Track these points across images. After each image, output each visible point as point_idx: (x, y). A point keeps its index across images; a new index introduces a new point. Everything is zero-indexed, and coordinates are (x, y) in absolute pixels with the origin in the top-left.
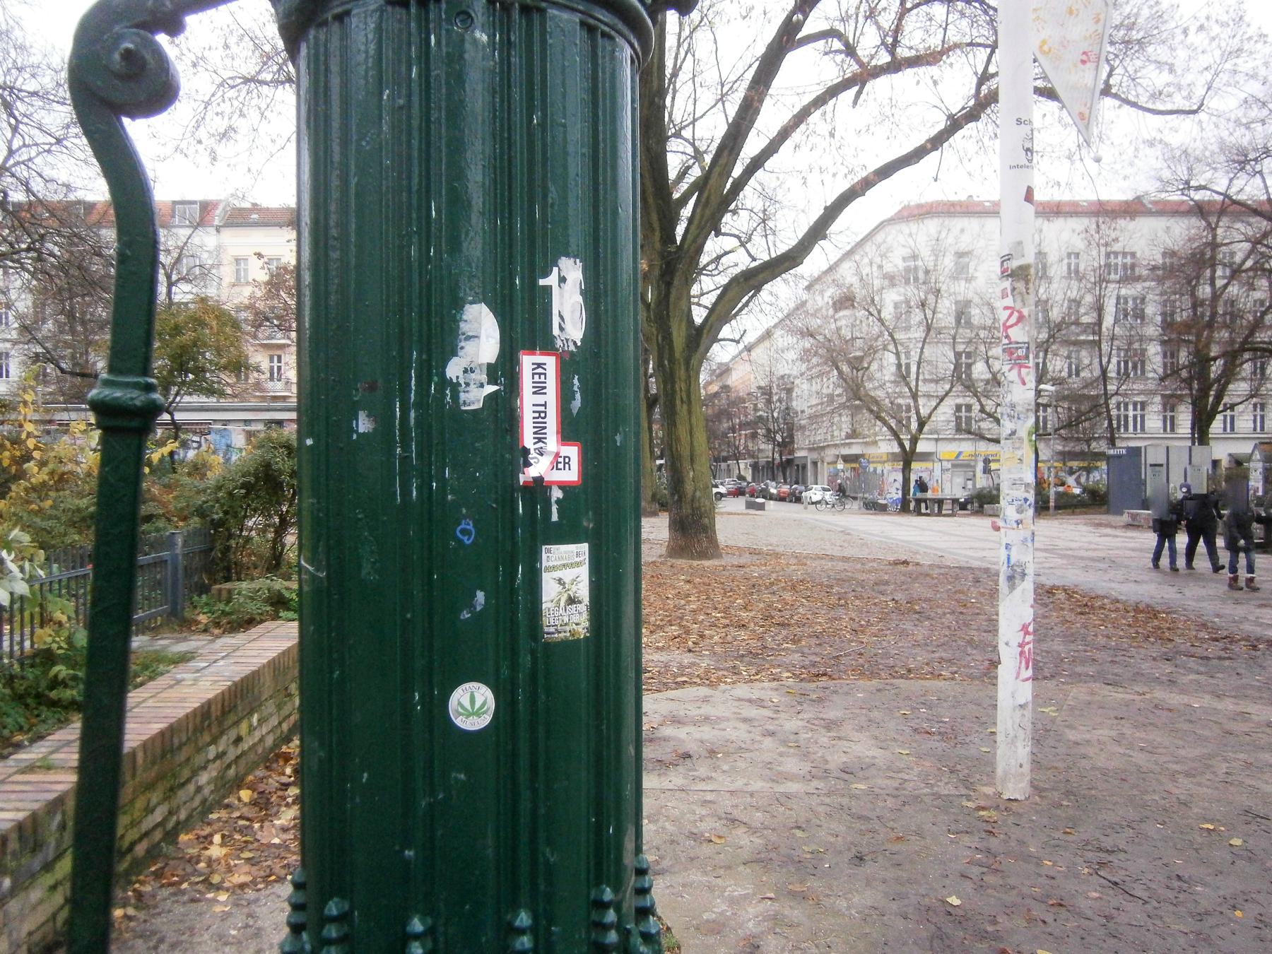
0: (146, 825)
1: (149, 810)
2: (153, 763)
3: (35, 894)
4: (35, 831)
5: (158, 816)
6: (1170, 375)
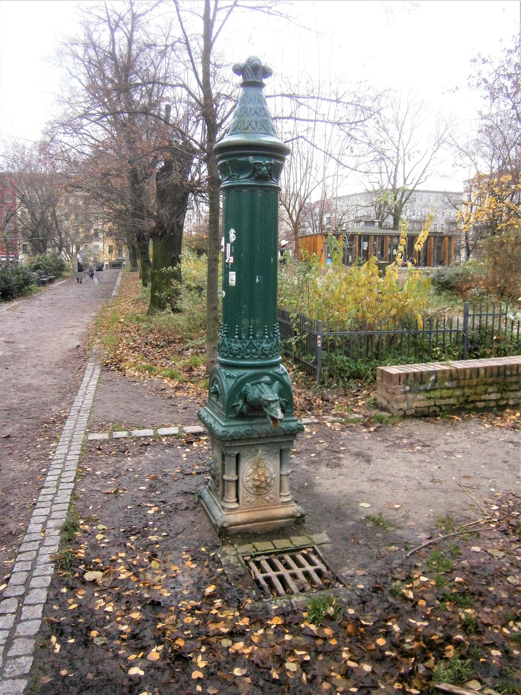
0: (483, 397)
1: (486, 392)
2: (491, 376)
3: (420, 397)
4: (422, 378)
5: (493, 396)
6: (515, 375)
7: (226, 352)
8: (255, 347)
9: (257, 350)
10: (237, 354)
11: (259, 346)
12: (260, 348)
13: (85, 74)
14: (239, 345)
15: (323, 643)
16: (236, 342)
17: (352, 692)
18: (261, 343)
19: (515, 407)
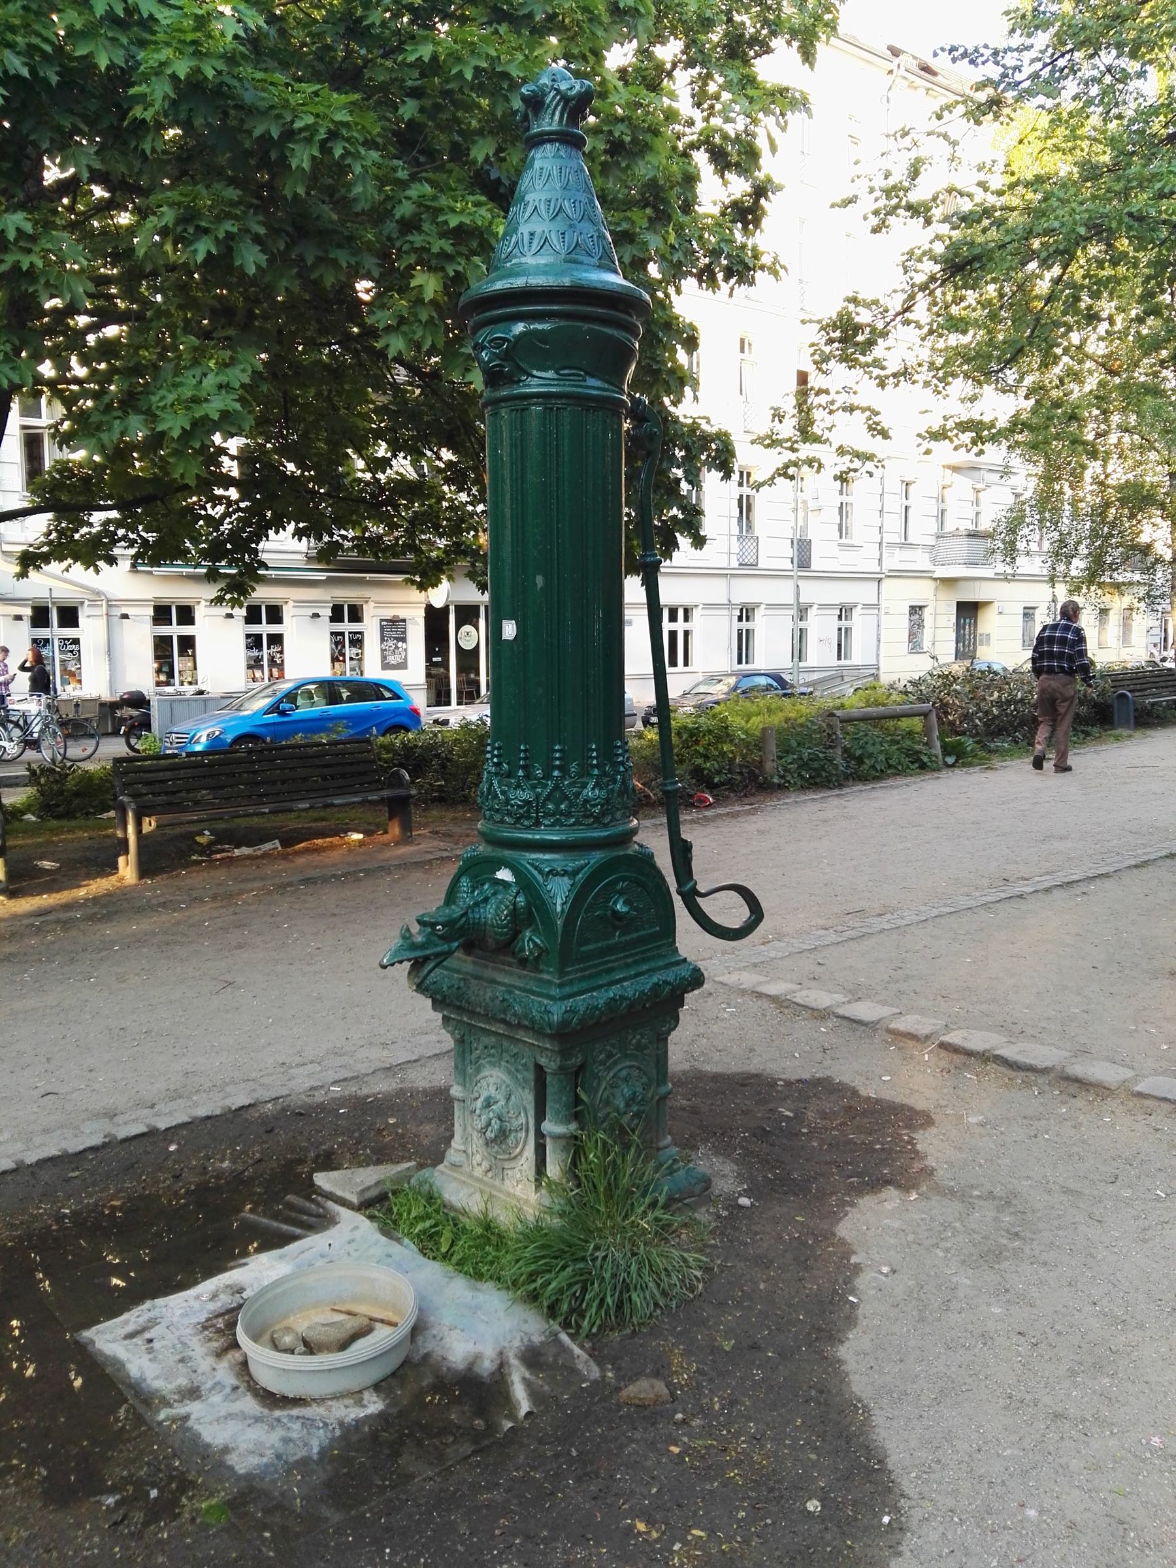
7: (497, 811)
8: (566, 797)
9: (571, 805)
10: (522, 816)
11: (577, 795)
12: (580, 801)
13: (903, 1496)
14: (526, 795)
15: (138, 222)
16: (518, 786)
17: (359, 832)
18: (584, 786)
19: (779, 4)
